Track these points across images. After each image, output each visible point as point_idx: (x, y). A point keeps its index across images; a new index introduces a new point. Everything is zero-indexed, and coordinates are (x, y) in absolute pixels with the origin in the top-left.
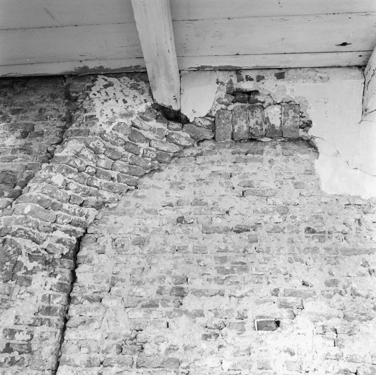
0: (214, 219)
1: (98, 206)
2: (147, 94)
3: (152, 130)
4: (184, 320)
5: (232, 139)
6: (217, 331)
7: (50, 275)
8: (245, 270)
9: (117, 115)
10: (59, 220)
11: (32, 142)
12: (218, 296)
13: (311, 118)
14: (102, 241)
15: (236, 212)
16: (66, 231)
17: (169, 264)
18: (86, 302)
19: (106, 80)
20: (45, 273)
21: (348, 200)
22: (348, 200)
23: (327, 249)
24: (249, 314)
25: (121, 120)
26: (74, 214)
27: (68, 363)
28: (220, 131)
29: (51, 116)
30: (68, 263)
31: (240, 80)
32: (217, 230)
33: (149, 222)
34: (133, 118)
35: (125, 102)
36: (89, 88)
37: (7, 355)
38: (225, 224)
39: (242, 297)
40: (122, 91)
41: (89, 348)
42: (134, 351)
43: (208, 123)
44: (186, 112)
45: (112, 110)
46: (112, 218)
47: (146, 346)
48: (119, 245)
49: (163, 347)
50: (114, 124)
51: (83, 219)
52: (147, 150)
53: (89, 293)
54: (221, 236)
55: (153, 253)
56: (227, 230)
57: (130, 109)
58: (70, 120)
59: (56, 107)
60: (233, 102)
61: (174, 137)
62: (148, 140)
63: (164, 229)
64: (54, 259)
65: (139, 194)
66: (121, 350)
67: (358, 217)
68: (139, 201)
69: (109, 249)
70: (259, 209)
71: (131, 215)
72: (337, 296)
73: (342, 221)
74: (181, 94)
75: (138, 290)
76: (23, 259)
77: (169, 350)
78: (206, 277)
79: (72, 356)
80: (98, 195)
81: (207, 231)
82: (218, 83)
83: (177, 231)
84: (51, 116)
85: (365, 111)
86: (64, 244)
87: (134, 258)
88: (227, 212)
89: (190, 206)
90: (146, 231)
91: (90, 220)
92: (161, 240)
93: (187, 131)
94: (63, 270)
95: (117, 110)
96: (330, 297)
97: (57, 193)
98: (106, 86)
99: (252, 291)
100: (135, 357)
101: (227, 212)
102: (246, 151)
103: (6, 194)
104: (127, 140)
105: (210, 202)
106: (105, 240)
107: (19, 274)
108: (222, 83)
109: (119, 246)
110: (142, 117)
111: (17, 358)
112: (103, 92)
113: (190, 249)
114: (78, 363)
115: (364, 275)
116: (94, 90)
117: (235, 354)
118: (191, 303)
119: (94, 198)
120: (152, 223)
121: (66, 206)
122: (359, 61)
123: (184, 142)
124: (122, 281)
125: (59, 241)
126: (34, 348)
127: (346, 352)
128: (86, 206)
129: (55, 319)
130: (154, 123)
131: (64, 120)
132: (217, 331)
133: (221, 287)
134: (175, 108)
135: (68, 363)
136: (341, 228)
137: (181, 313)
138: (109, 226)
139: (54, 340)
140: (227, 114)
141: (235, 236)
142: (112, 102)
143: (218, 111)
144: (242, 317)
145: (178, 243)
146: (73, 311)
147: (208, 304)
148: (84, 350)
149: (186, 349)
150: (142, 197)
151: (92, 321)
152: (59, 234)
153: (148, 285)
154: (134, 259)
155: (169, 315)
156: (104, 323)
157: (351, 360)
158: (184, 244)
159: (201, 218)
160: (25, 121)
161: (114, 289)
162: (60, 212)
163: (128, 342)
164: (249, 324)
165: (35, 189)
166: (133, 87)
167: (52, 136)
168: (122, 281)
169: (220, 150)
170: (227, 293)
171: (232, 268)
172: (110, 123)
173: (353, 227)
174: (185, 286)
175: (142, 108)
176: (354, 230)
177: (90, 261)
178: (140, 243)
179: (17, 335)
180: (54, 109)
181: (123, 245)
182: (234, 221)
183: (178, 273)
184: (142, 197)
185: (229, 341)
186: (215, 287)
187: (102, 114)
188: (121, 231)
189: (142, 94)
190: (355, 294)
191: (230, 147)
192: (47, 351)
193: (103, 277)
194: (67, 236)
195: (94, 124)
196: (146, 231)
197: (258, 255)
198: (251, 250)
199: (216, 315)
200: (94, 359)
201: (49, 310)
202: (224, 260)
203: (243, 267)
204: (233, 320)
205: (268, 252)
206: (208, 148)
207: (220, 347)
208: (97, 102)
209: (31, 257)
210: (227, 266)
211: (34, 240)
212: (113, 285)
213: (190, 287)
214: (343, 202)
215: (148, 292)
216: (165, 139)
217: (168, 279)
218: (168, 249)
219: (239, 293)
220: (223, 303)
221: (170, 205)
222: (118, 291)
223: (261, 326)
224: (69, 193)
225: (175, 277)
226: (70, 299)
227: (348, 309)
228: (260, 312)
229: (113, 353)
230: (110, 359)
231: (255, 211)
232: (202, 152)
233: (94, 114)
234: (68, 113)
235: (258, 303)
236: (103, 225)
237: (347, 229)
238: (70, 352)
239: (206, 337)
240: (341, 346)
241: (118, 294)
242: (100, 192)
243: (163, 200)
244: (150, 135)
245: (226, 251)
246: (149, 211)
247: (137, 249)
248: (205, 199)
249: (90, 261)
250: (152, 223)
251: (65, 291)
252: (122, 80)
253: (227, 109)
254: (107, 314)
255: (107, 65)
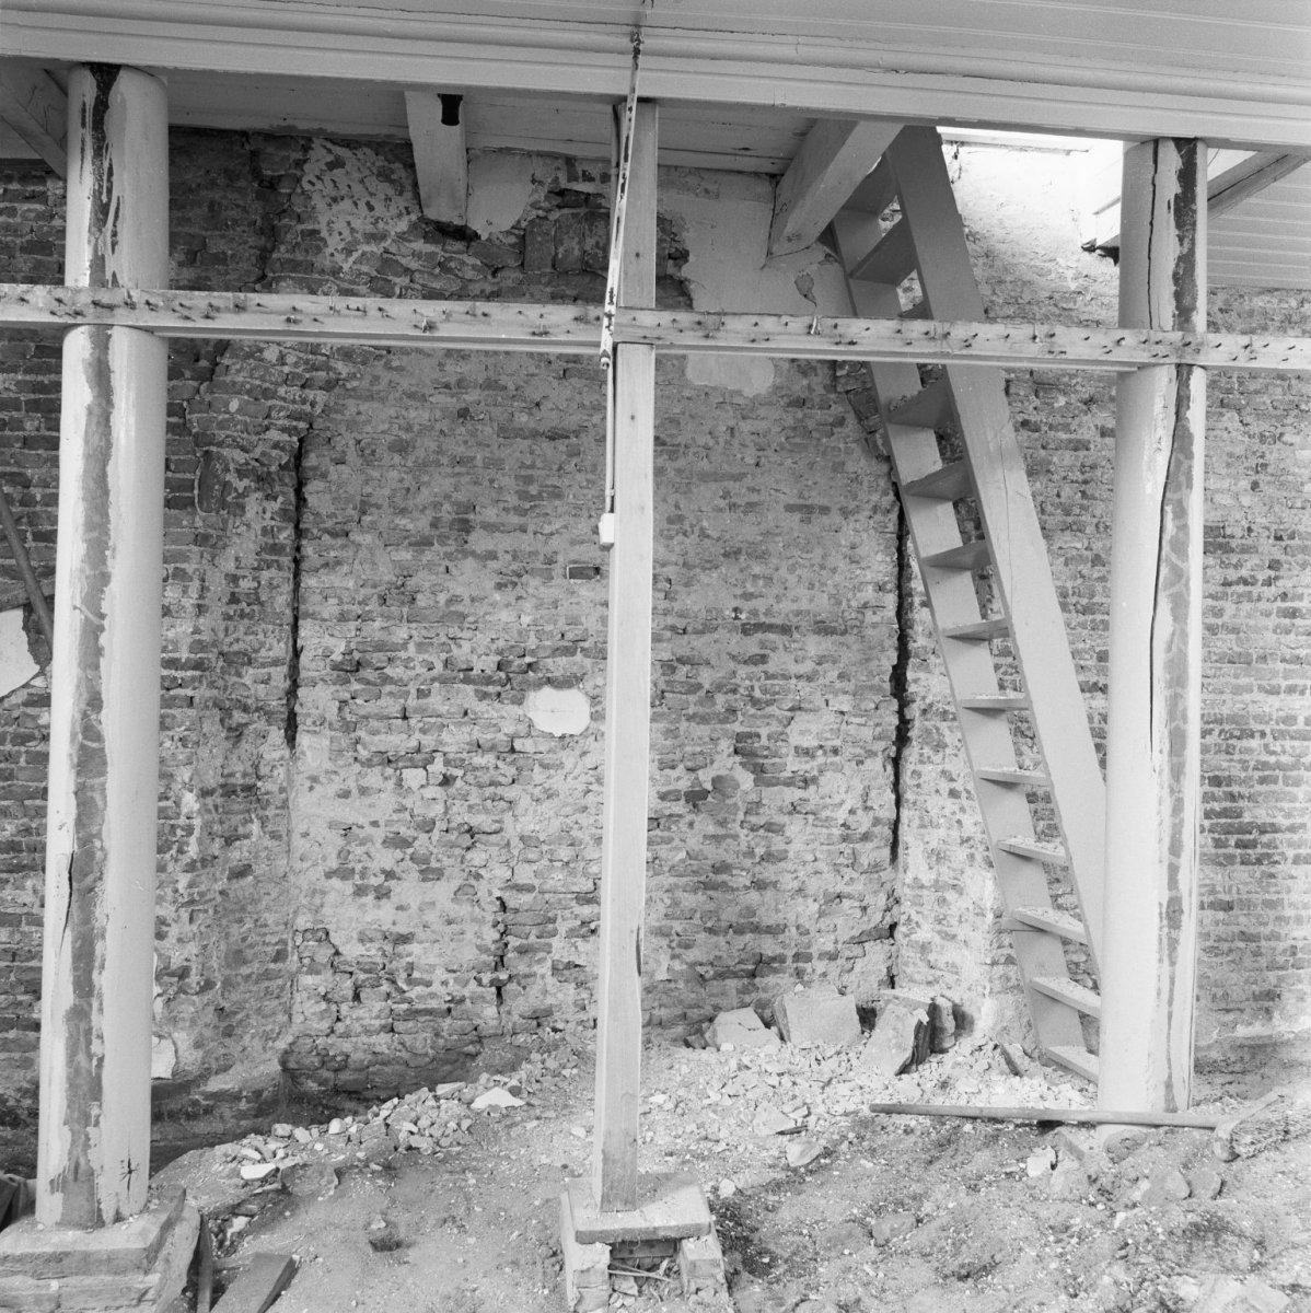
0: (517, 415)
1: (329, 386)
2: (408, 195)
3: (416, 255)
4: (470, 563)
5: (553, 266)
6: (515, 579)
7: (267, 497)
8: (559, 496)
9: (359, 236)
10: (274, 414)
11: (210, 274)
12: (518, 533)
13: (689, 246)
14: (339, 443)
15: (550, 406)
16: (284, 430)
17: (447, 484)
18: (326, 537)
19: (329, 151)
20: (259, 495)
21: (723, 395)
22: (723, 395)
23: (679, 471)
24: (560, 558)
25: (367, 248)
26: (294, 402)
27: (312, 616)
28: (532, 254)
29: (235, 222)
30: (290, 478)
31: (572, 178)
32: (520, 433)
33: (413, 414)
34: (387, 243)
35: (371, 208)
36: (299, 164)
37: (234, 606)
38: (532, 425)
39: (552, 534)
40: (362, 181)
41: (340, 599)
42: (403, 603)
43: (513, 240)
44: (477, 225)
45: (349, 223)
46: (352, 406)
47: (419, 596)
48: (368, 452)
49: (442, 598)
50: (355, 255)
51: (307, 408)
52: (407, 288)
53: (329, 524)
54: (527, 442)
55: (423, 466)
56: (535, 434)
57: (381, 225)
58: (272, 233)
59: (241, 203)
60: (559, 207)
61: (452, 265)
62: (407, 271)
63: (438, 426)
64: (269, 473)
65: (394, 364)
66: (383, 600)
67: (732, 423)
68: (395, 376)
69: (352, 456)
70: (587, 403)
71: (383, 400)
72: (680, 537)
73: (706, 428)
74: (468, 195)
75: (402, 522)
76: (231, 477)
77: (450, 602)
78: (501, 505)
79: (317, 609)
80: (329, 369)
81: (507, 432)
82: (533, 181)
83: (458, 432)
84: (235, 222)
85: (769, 253)
86: (283, 449)
87: (391, 476)
88: (538, 405)
89: (478, 391)
90: (409, 429)
91: (318, 410)
92: (433, 446)
93: (476, 255)
94: (285, 489)
95: (357, 224)
96: (672, 538)
97: (271, 374)
98: (332, 166)
99: (566, 527)
100: (405, 610)
101: (538, 405)
102: (574, 293)
103: (188, 374)
104: (374, 273)
105: (511, 386)
106: (345, 442)
107: (229, 499)
108: (541, 183)
109: (368, 455)
110: (401, 237)
111: (247, 610)
112: (327, 178)
113: (479, 461)
114: (326, 616)
115: (721, 510)
116: (311, 170)
117: (537, 607)
118: (479, 541)
119: (322, 374)
120: (418, 415)
121: (282, 391)
122: (767, 167)
123: (470, 274)
124: (379, 507)
125: (276, 446)
126: (263, 598)
127: (677, 606)
128: (310, 387)
129: (286, 561)
130: (419, 245)
131: (262, 232)
132: (515, 579)
133: (522, 520)
134: (457, 222)
135: (312, 616)
136: (703, 440)
137: (466, 554)
138: (347, 417)
139: (287, 588)
140: (546, 226)
141: (546, 445)
142: (346, 205)
143: (532, 222)
144: (550, 561)
145: (461, 450)
146: (309, 549)
147: (502, 543)
148: (333, 601)
149: (473, 600)
150: (400, 369)
151: (338, 563)
152: (274, 435)
153: (416, 514)
154: (394, 474)
155: (448, 556)
156: (357, 566)
157: (681, 615)
158: (469, 454)
159: (496, 411)
160: (186, 229)
161: (367, 519)
162: (274, 402)
163: (394, 591)
164: (557, 570)
165: (238, 371)
166: (384, 176)
167: (244, 266)
168: (379, 507)
169: (533, 288)
170: (531, 528)
171: (540, 493)
172: (348, 252)
173: (721, 440)
174: (471, 516)
175: (403, 225)
176: (722, 444)
177: (324, 476)
178: (401, 448)
179: (241, 582)
180: (238, 206)
181: (373, 452)
182: (548, 418)
183: (460, 497)
184: (400, 369)
185: (531, 591)
186: (515, 519)
187: (330, 232)
188: (369, 429)
189: (401, 194)
190: (704, 535)
191: (548, 284)
192: (282, 600)
193: (348, 501)
194: (286, 437)
195: (319, 250)
196: (409, 429)
197: (579, 477)
198: (570, 467)
199: (515, 558)
200: (348, 612)
201: (276, 549)
202: (529, 480)
203: (557, 494)
204: (538, 565)
205: (593, 472)
206: (509, 283)
207: (519, 598)
208: (319, 202)
209: (241, 474)
210: (533, 490)
211: (244, 449)
212: (364, 513)
213: (479, 518)
214: (715, 399)
215: (418, 524)
216: (437, 270)
217: (447, 506)
218: (445, 460)
219: (547, 529)
220: (526, 542)
221: (447, 386)
222: (372, 522)
223: (575, 574)
224: (286, 369)
225: (457, 504)
226: (299, 533)
227: (692, 554)
228: (573, 556)
229: (373, 605)
230: (370, 612)
231: (582, 406)
232: (500, 290)
233: (316, 227)
234: (265, 217)
235: (573, 543)
236: (339, 417)
237: (711, 443)
238: (312, 603)
239: (500, 586)
240: (674, 599)
241: (373, 527)
242: (332, 363)
243: (435, 376)
244: (414, 265)
245: (532, 466)
246: (411, 396)
247: (397, 459)
248: (504, 380)
249: (324, 476)
250: (418, 415)
251: (290, 520)
252: (359, 153)
253: (546, 218)
254: (360, 555)
255: (330, 128)
